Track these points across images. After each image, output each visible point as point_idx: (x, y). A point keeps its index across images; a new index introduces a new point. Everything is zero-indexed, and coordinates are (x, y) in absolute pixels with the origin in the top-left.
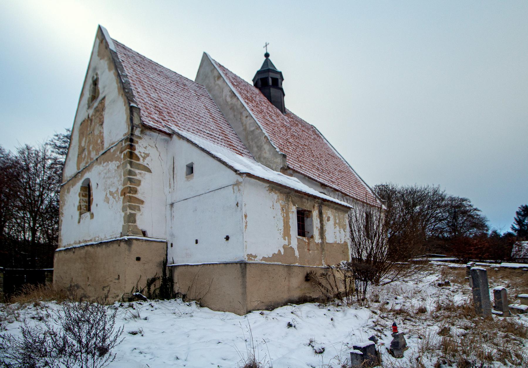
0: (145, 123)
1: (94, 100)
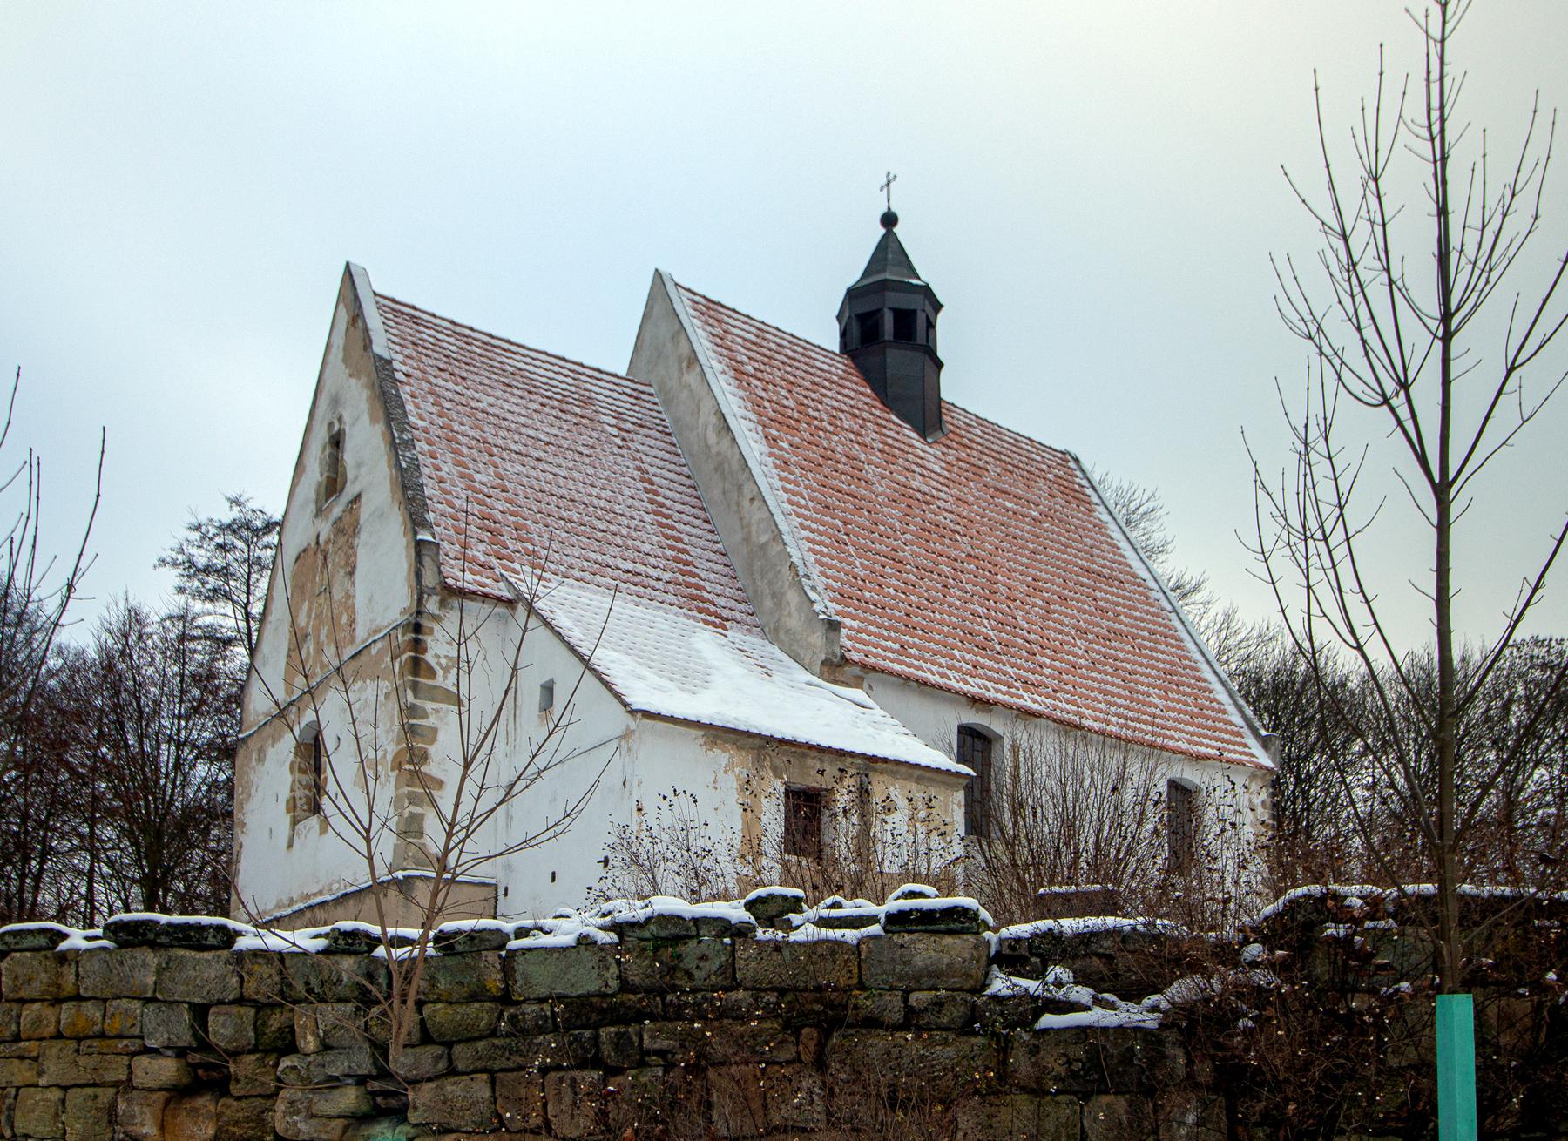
0: (450, 581)
1: (331, 496)
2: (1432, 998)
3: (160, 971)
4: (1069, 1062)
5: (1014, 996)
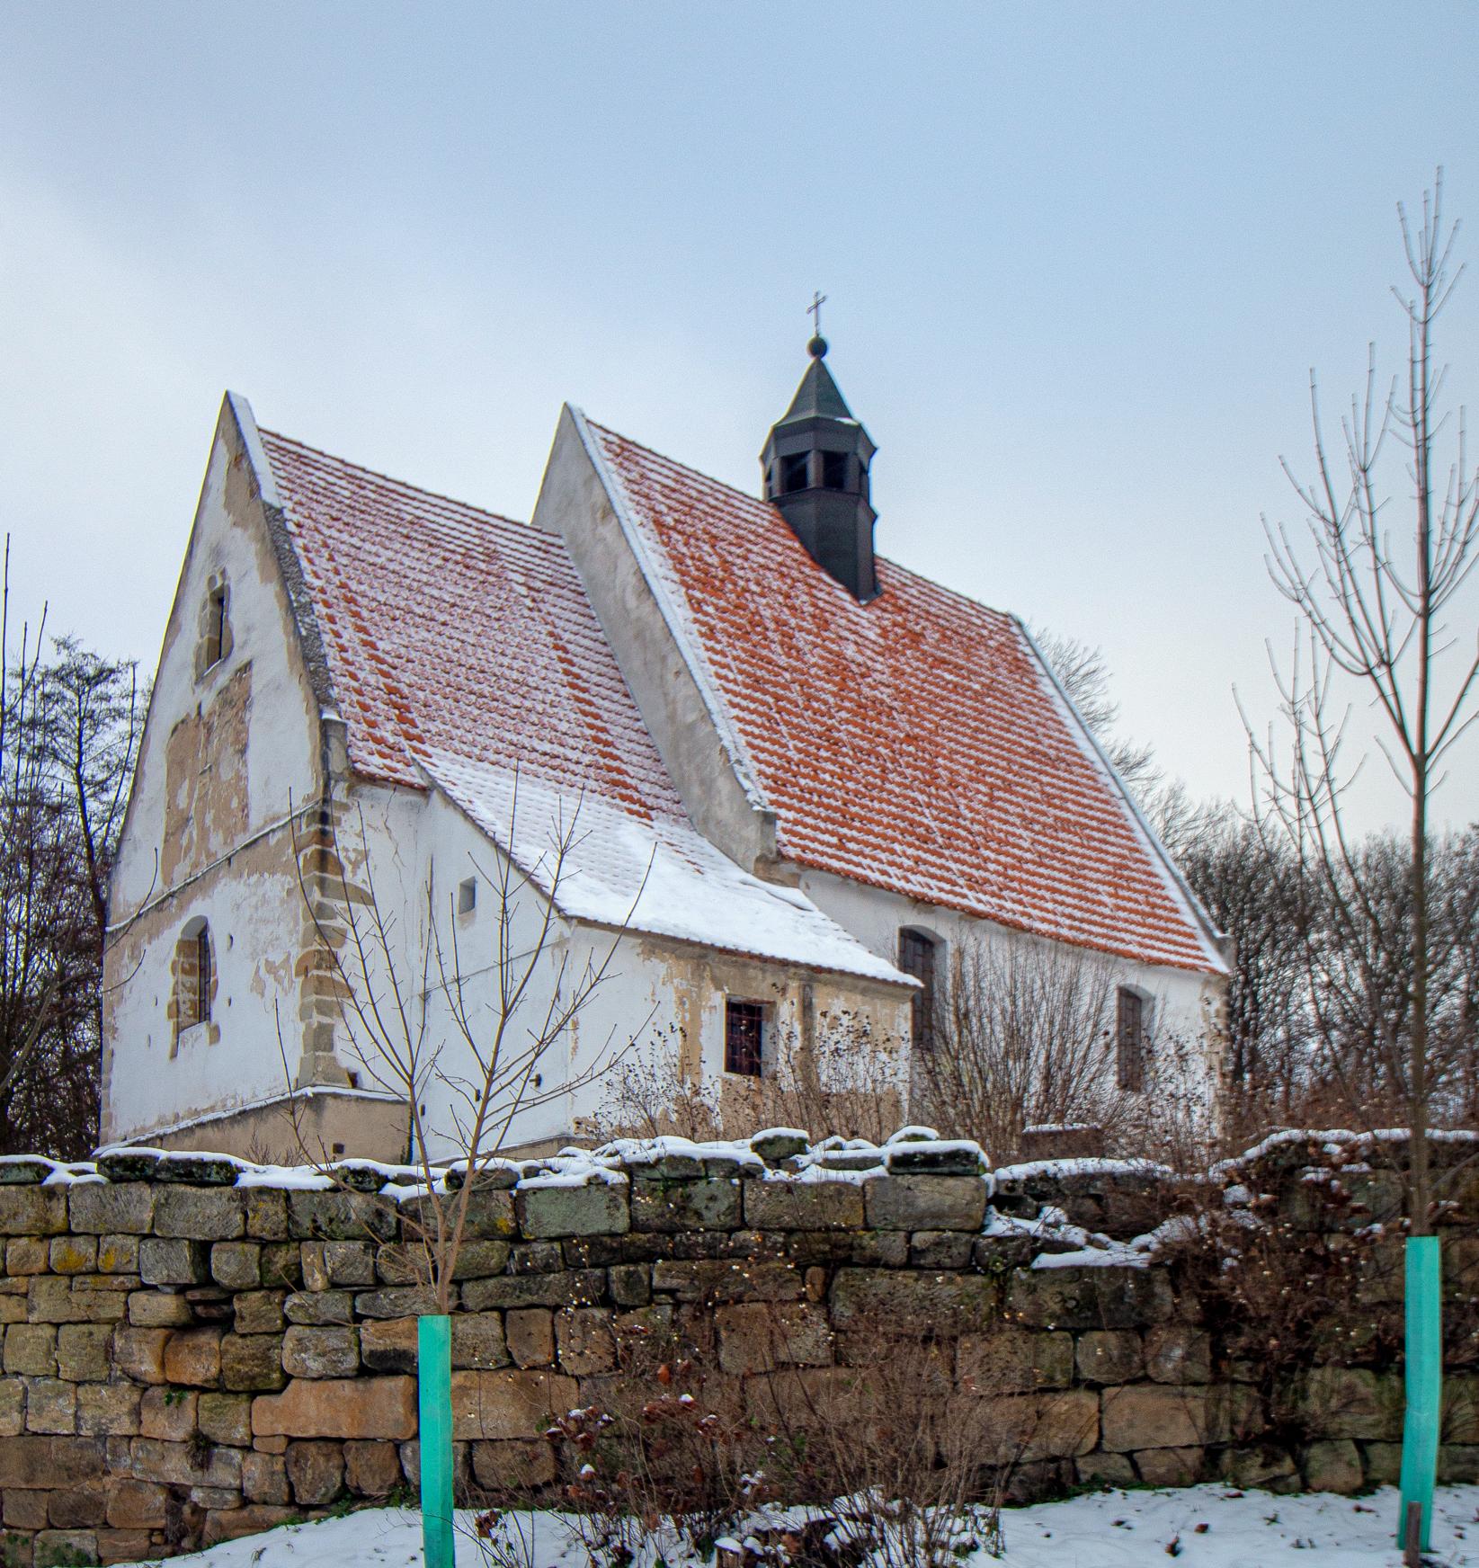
0: (359, 766)
2: (1402, 1240)
3: (158, 1207)
4: (1064, 1301)
5: (1012, 1239)
